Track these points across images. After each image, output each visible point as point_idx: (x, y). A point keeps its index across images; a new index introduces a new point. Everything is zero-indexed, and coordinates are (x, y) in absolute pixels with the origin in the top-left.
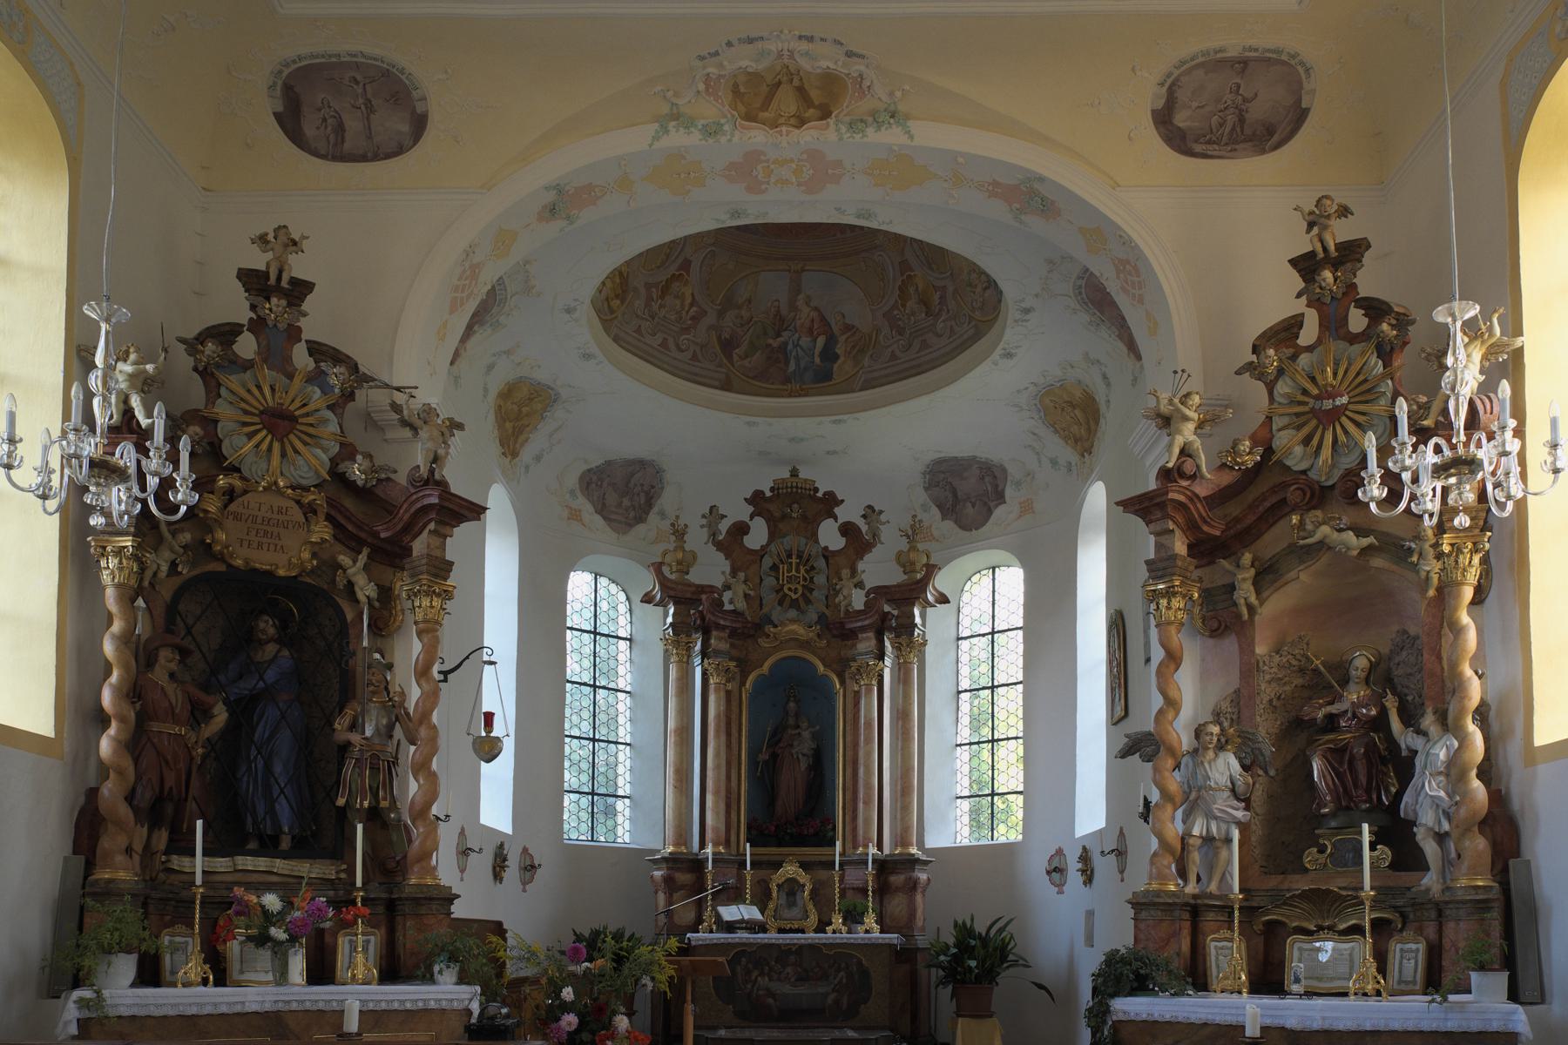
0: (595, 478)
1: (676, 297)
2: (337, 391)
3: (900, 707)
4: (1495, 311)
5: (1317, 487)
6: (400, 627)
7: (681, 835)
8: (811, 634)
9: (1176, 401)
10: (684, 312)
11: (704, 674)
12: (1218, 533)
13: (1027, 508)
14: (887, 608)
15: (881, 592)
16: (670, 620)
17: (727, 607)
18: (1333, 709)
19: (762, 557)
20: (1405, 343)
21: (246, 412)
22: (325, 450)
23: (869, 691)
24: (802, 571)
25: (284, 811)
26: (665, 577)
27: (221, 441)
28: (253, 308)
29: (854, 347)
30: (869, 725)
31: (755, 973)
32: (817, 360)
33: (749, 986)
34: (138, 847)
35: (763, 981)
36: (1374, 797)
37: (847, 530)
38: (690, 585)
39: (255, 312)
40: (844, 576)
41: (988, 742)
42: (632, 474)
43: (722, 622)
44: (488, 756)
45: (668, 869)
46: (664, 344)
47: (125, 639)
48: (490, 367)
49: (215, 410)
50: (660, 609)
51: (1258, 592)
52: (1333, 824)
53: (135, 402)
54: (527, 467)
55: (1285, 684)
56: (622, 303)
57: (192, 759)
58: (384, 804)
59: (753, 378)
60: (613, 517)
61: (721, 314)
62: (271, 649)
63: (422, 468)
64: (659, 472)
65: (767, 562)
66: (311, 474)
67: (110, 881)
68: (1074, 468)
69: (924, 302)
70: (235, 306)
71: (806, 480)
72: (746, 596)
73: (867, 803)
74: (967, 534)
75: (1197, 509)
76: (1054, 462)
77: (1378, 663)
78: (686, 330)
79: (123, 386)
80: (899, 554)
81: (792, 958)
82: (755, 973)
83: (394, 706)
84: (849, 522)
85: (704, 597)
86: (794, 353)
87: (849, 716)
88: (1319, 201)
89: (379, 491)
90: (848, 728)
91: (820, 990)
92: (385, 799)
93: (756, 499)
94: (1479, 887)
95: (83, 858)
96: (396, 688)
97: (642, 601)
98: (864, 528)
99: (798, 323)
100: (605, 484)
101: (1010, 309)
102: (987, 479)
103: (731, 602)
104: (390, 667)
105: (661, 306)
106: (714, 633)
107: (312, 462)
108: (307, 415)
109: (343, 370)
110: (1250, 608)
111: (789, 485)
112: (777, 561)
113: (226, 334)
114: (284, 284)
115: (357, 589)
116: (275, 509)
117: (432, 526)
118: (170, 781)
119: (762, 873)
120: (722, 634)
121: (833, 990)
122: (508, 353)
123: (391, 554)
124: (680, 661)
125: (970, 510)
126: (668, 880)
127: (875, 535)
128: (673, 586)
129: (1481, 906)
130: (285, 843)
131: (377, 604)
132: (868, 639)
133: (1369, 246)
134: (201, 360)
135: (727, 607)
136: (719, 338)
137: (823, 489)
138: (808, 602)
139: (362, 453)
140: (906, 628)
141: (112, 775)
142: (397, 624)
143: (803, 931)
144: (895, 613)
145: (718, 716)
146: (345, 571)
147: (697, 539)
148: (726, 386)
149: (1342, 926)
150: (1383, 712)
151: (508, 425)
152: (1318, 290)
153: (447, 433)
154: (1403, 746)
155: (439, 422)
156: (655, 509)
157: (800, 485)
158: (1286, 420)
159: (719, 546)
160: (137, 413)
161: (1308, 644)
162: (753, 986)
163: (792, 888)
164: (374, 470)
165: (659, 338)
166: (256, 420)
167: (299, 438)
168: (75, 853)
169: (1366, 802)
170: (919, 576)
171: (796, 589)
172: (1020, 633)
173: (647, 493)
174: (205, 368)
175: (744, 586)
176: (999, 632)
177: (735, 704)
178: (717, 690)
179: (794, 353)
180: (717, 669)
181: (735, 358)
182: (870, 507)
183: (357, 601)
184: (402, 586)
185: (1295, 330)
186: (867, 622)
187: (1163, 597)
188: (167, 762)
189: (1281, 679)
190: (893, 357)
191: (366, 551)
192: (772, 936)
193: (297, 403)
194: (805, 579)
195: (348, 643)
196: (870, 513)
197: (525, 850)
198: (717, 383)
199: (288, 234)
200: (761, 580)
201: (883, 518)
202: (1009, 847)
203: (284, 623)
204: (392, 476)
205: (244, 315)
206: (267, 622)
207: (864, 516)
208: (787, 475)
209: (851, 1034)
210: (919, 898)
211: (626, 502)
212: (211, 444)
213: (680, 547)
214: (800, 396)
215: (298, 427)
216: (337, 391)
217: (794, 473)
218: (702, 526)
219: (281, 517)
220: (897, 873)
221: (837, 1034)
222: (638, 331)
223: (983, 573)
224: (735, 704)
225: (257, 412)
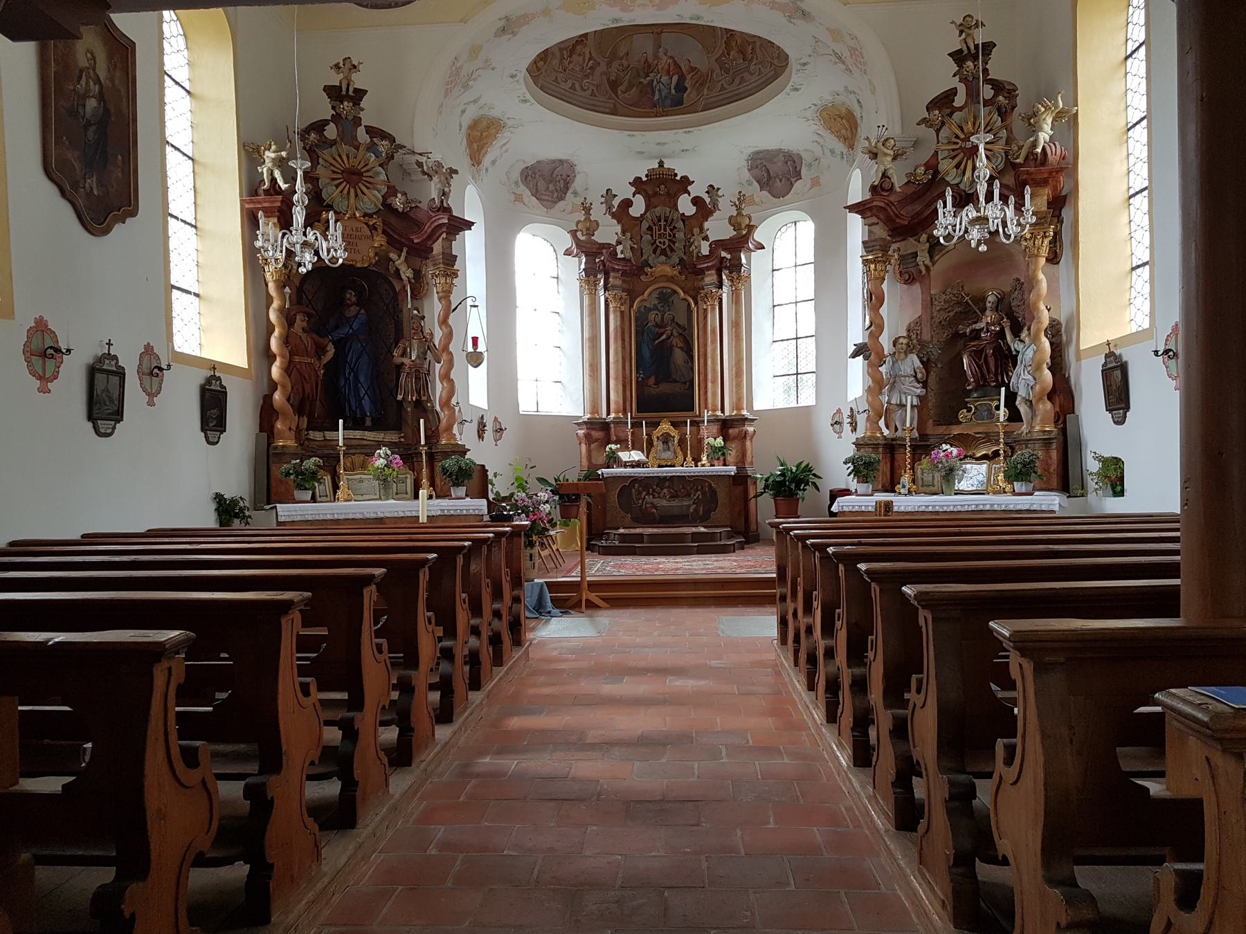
1: (580, 55)
2: (383, 155)
4: (1059, 93)
5: (963, 194)
6: (426, 294)
7: (594, 407)
9: (880, 144)
10: (585, 65)
11: (606, 301)
12: (906, 223)
13: (816, 182)
14: (723, 254)
15: (718, 245)
16: (583, 266)
17: (620, 256)
18: (977, 326)
19: (641, 222)
20: (1013, 108)
21: (334, 172)
22: (379, 191)
23: (713, 309)
24: (668, 230)
25: (366, 402)
26: (579, 239)
27: (321, 190)
28: (333, 108)
29: (697, 82)
30: (713, 331)
31: (644, 493)
32: (673, 91)
33: (640, 502)
34: (294, 428)
35: (649, 499)
36: (1000, 379)
37: (697, 201)
38: (595, 243)
39: (335, 111)
40: (695, 233)
44: (476, 364)
45: (587, 429)
46: (573, 87)
47: (281, 310)
48: (463, 112)
49: (317, 172)
50: (577, 259)
51: (931, 257)
52: (975, 395)
53: (277, 174)
54: (487, 170)
55: (949, 312)
56: (545, 63)
57: (318, 376)
58: (424, 398)
59: (631, 105)
60: (543, 197)
61: (609, 64)
62: (354, 309)
63: (436, 200)
64: (572, 166)
66: (373, 205)
67: (283, 447)
68: (845, 156)
69: (742, 52)
70: (324, 110)
71: (669, 169)
72: (632, 248)
73: (714, 382)
74: (778, 200)
75: (892, 210)
76: (832, 152)
77: (1002, 299)
78: (587, 76)
79: (270, 165)
80: (730, 218)
81: (667, 484)
82: (644, 493)
83: (426, 341)
85: (604, 251)
86: (658, 88)
87: (701, 326)
88: (964, 18)
89: (411, 214)
90: (700, 334)
91: (685, 503)
92: (424, 395)
93: (637, 182)
94: (1045, 431)
95: (266, 434)
96: (427, 331)
98: (708, 200)
99: (660, 67)
100: (537, 176)
101: (794, 63)
102: (789, 163)
103: (622, 252)
104: (423, 318)
105: (570, 62)
106: (612, 274)
107: (372, 199)
108: (368, 171)
109: (387, 143)
110: (927, 268)
112: (652, 224)
113: (319, 126)
114: (351, 93)
115: (401, 272)
116: (354, 229)
117: (444, 235)
118: (308, 390)
120: (617, 275)
121: (694, 503)
122: (475, 101)
123: (420, 252)
124: (591, 293)
126: (587, 436)
129: (1047, 442)
130: (368, 423)
131: (413, 281)
132: (711, 275)
133: (995, 45)
134: (307, 144)
135: (620, 256)
136: (608, 80)
138: (672, 250)
139: (400, 193)
141: (279, 387)
142: (425, 291)
143: (674, 466)
144: (729, 256)
145: (616, 328)
146: (394, 262)
147: (598, 213)
148: (614, 112)
149: (978, 455)
150: (1002, 329)
151: (475, 146)
152: (965, 73)
153: (449, 177)
154: (1013, 349)
155: (444, 171)
156: (571, 190)
158: (946, 153)
159: (614, 216)
160: (278, 181)
161: (962, 287)
163: (666, 439)
164: (408, 201)
165: (570, 83)
166: (340, 176)
167: (366, 186)
168: (260, 431)
169: (994, 382)
170: (744, 232)
172: (813, 265)
173: (565, 180)
174: (310, 148)
177: (626, 319)
178: (615, 312)
179: (658, 88)
180: (614, 298)
181: (619, 92)
182: (711, 186)
183: (402, 280)
184: (429, 271)
185: (951, 98)
186: (710, 264)
187: (872, 263)
188: (305, 379)
189: (946, 309)
190: (723, 88)
191: (405, 250)
192: (653, 471)
193: (362, 164)
194: (670, 236)
195: (398, 305)
196: (712, 190)
197: (496, 419)
198: (607, 110)
199: (351, 62)
200: (642, 237)
201: (720, 193)
202: (807, 409)
203: (359, 295)
204: (418, 205)
205: (328, 113)
206: (351, 294)
207: (707, 192)
208: (657, 166)
209: (702, 529)
210: (748, 443)
211: (551, 187)
212: (315, 192)
213: (588, 219)
214: (662, 116)
215: (364, 179)
216: (383, 155)
217: (661, 164)
218: (602, 203)
219: (358, 234)
221: (694, 530)
222: (556, 80)
223: (788, 225)
225: (340, 171)
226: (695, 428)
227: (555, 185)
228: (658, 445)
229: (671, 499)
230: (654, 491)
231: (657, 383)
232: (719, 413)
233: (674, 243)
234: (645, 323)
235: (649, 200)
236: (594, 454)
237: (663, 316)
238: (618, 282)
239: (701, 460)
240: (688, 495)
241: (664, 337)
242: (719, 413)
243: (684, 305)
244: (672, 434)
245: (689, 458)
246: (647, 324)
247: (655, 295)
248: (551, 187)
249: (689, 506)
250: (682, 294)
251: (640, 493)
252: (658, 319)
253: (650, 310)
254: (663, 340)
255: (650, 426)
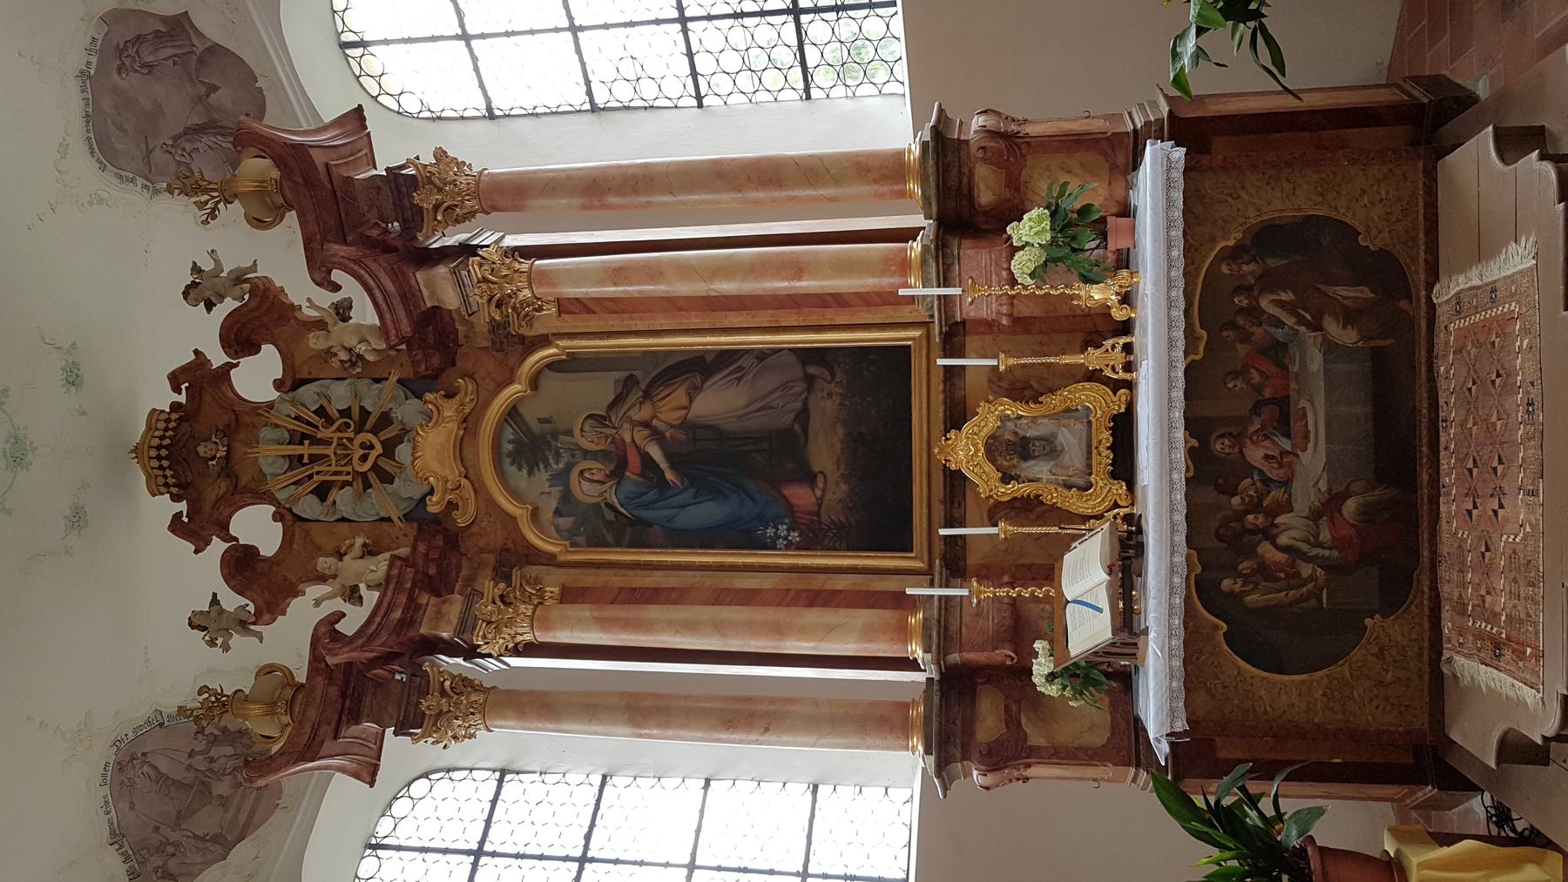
0: (157, 861)
3: (576, 201)
8: (448, 413)
11: (517, 652)
30: (617, 275)
33: (1306, 570)
35: (1291, 529)
37: (239, 339)
41: (685, 31)
42: (161, 777)
43: (397, 614)
45: (966, 756)
65: (308, 507)
72: (369, 551)
73: (798, 269)
74: (269, 99)
80: (258, 223)
81: (1220, 446)
82: (1267, 550)
84: (222, 340)
91: (1316, 362)
97: (372, 784)
98: (229, 305)
100: (174, 836)
102: (150, 59)
111: (155, 463)
119: (971, 509)
121: (1316, 326)
125: (223, 97)
127: (239, 278)
128: (308, 728)
132: (430, 285)
137: (165, 398)
138: (385, 419)
140: (399, 183)
145: (604, 624)
157: (156, 442)
162: (1308, 559)
171: (363, 446)
173: (214, 741)
175: (346, 558)
176: (462, 25)
178: (547, 625)
182: (186, 294)
196: (200, 291)
200: (343, 519)
201: (207, 265)
207: (209, 306)
220: (971, 188)
224: (590, 579)
226: (972, 342)
227: (219, 776)
228: (1041, 478)
229: (1296, 427)
230: (1256, 507)
231: (809, 478)
232: (915, 248)
233: (365, 413)
234: (610, 516)
235: (246, 490)
236: (1066, 734)
237: (586, 454)
238: (454, 607)
239: (1104, 313)
240: (1276, 352)
241: (655, 452)
242: (915, 248)
243: (551, 383)
244: (992, 424)
245: (1092, 359)
246: (610, 507)
247: (519, 477)
248: (222, 788)
249: (1331, 349)
250: (516, 387)
251: (1265, 571)
252: (598, 469)
253: (567, 498)
254: (668, 456)
255: (962, 503)
